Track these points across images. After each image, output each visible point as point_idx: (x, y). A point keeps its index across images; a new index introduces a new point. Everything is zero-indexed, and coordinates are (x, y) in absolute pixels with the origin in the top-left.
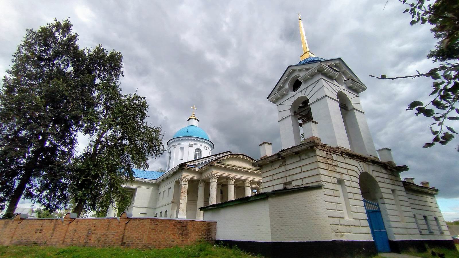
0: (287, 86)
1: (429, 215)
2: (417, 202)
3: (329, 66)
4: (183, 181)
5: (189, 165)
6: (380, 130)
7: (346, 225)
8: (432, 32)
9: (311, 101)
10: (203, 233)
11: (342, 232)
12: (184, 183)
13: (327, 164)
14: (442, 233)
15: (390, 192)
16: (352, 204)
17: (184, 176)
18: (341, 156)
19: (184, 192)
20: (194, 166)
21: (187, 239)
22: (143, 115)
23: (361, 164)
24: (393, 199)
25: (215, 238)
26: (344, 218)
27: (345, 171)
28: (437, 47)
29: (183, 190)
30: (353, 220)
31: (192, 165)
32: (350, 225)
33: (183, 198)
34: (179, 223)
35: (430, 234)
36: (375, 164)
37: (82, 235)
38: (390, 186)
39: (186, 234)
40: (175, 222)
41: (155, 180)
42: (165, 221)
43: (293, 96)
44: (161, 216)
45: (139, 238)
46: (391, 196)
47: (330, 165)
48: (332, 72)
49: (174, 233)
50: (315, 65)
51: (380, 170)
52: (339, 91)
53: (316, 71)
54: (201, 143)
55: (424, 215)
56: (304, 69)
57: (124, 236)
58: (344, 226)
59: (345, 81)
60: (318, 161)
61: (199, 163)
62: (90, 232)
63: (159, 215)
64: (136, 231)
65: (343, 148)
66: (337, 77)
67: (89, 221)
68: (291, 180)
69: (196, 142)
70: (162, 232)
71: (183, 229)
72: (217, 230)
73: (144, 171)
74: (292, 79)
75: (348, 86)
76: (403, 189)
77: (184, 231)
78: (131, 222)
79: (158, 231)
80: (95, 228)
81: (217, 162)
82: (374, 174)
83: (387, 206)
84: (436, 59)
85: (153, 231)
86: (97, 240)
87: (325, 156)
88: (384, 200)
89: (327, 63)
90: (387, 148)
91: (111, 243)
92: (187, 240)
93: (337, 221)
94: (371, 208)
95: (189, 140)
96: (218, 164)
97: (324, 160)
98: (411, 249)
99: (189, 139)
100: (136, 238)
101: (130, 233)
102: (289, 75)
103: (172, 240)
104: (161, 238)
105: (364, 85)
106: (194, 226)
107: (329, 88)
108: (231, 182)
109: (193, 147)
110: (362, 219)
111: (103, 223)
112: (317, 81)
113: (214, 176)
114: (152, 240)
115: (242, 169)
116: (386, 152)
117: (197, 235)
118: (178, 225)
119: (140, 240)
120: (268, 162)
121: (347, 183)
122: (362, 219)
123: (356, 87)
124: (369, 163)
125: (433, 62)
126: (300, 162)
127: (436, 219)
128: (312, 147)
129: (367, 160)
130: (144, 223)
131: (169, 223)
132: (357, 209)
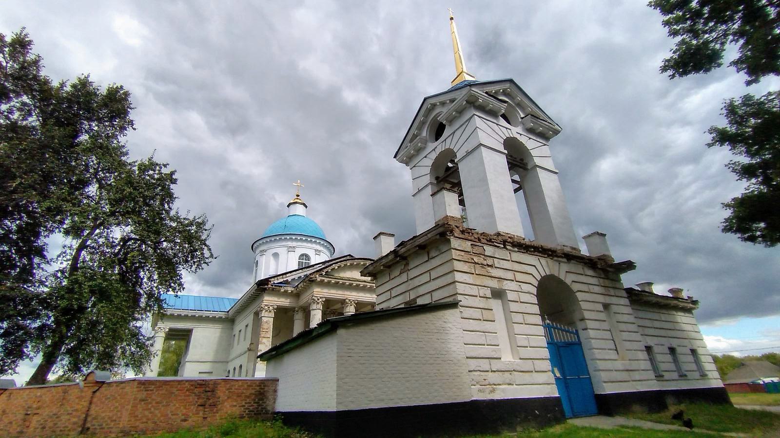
0: (424, 134)
1: (679, 346)
2: (657, 324)
3: (486, 93)
4: (264, 311)
5: (274, 283)
6: (642, 209)
7: (504, 371)
8: (664, 27)
9: (459, 155)
10: (248, 401)
11: (495, 385)
12: (266, 314)
13: (473, 263)
14: (704, 376)
15: (600, 307)
16: (518, 333)
17: (265, 303)
18: (503, 248)
19: (267, 330)
20: (284, 284)
21: (216, 414)
22: (169, 196)
23: (543, 261)
24: (605, 321)
25: (274, 408)
26: (500, 358)
27: (510, 275)
28: (672, 51)
29: (265, 326)
30: (519, 360)
31: (281, 283)
32: (511, 371)
33: (264, 340)
34: (198, 386)
35: (681, 378)
36: (572, 261)
37: (14, 419)
38: (601, 299)
39: (214, 405)
40: (191, 383)
41: (226, 313)
42: (171, 383)
43: (434, 150)
44: (234, 375)
45: (114, 418)
46: (602, 316)
47: (478, 266)
48: (493, 104)
49: (188, 404)
50: (462, 92)
51: (582, 269)
52: (509, 136)
53: (465, 102)
54: (309, 245)
55: (670, 346)
56: (448, 102)
57: (87, 416)
58: (500, 373)
59: (522, 118)
60: (454, 259)
61: (299, 275)
62: (29, 413)
63: (232, 375)
64: (110, 405)
65: (507, 234)
66: (504, 111)
67: (30, 392)
68: (416, 297)
69: (300, 244)
70: (161, 405)
71: (208, 396)
72: (278, 394)
73: (176, 296)
74: (432, 119)
75: (527, 127)
76: (626, 301)
77: (210, 399)
78: (103, 389)
79: (154, 402)
80: (40, 404)
81: (322, 274)
82: (568, 279)
83: (592, 333)
84: (675, 73)
85: (143, 403)
86: (40, 427)
87: (469, 249)
88: (585, 322)
89: (485, 89)
90: (598, 233)
91: (65, 430)
92: (214, 416)
93: (484, 365)
94: (568, 339)
95: (283, 239)
96: (323, 278)
97: (466, 257)
98: (636, 408)
99: (288, 238)
100: (109, 418)
101: (100, 409)
102: (427, 115)
103: (183, 417)
104: (159, 415)
105: (557, 124)
106: (232, 389)
107: (489, 131)
108: (348, 308)
109: (294, 251)
110: (538, 359)
111: (54, 394)
112: (468, 119)
113: (316, 299)
114: (139, 420)
115: (367, 284)
116: (597, 239)
117: (236, 406)
118: (196, 389)
119: (115, 421)
120: (382, 268)
121: (511, 296)
122: (538, 359)
123: (541, 128)
124: (560, 259)
125: (670, 79)
126: (428, 262)
127: (694, 352)
128: (443, 235)
129: (555, 254)
130: (125, 390)
131: (177, 388)
132: (528, 339)
